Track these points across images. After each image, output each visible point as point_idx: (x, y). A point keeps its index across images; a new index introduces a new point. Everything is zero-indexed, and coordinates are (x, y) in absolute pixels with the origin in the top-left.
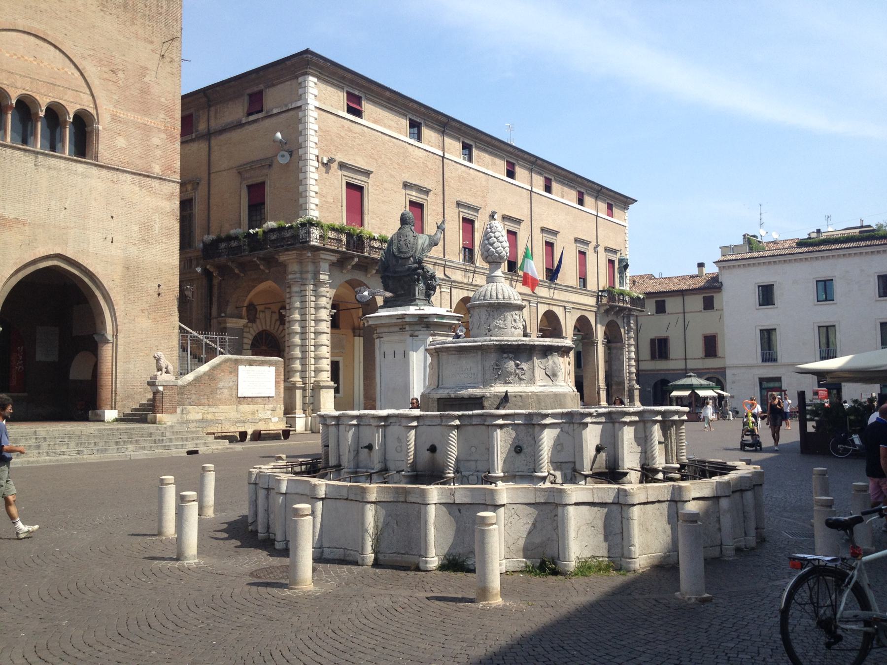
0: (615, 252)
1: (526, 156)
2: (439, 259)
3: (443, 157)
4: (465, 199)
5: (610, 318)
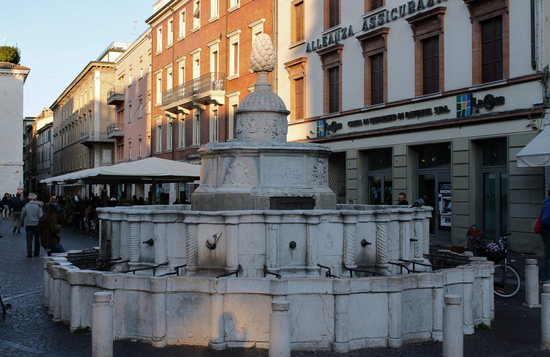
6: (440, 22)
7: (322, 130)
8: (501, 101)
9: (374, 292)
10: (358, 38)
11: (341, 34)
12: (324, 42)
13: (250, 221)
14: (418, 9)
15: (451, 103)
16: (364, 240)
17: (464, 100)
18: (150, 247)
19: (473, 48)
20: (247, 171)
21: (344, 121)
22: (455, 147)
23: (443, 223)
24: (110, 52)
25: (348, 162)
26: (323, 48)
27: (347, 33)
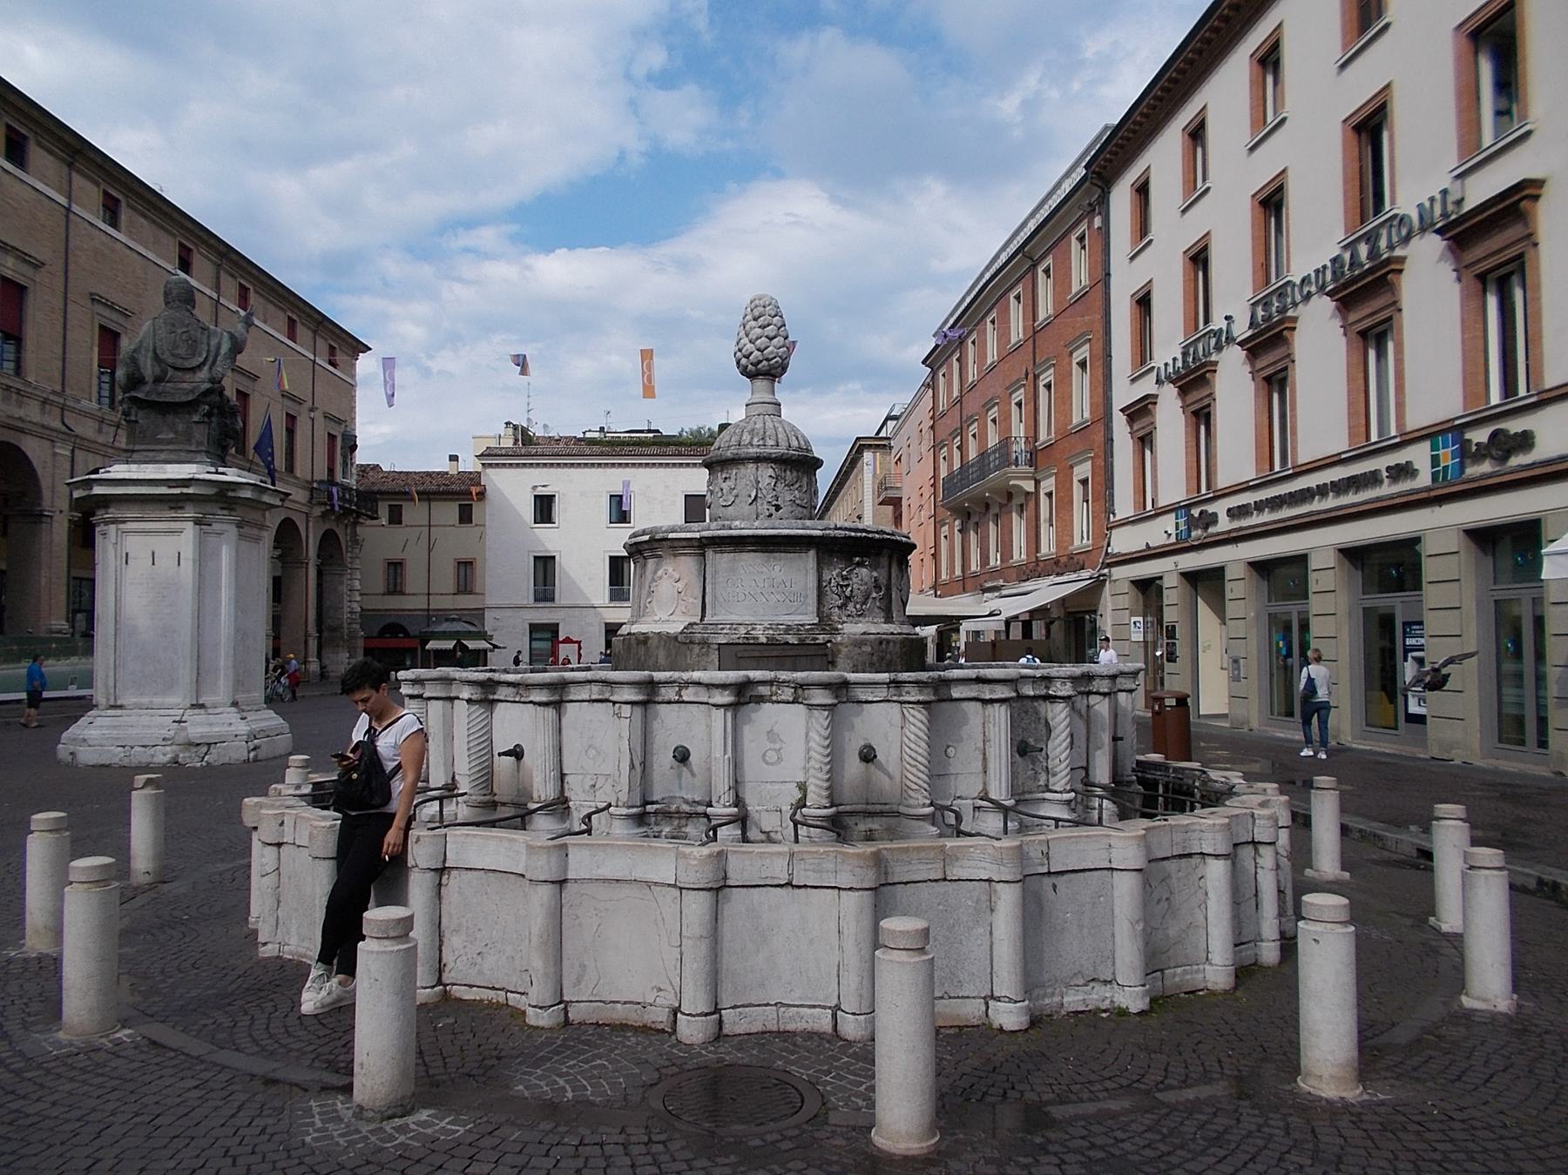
0: (339, 422)
1: (212, 241)
2: (54, 392)
3: (68, 210)
4: (101, 290)
5: (327, 526)
7: (1183, 527)
8: (1525, 441)
9: (799, 887)
11: (1213, 341)
12: (1184, 362)
13: (586, 697)
15: (1419, 455)
16: (870, 748)
19: (1463, 333)
20: (680, 585)
21: (1220, 508)
22: (1429, 547)
23: (1414, 708)
25: (1228, 586)
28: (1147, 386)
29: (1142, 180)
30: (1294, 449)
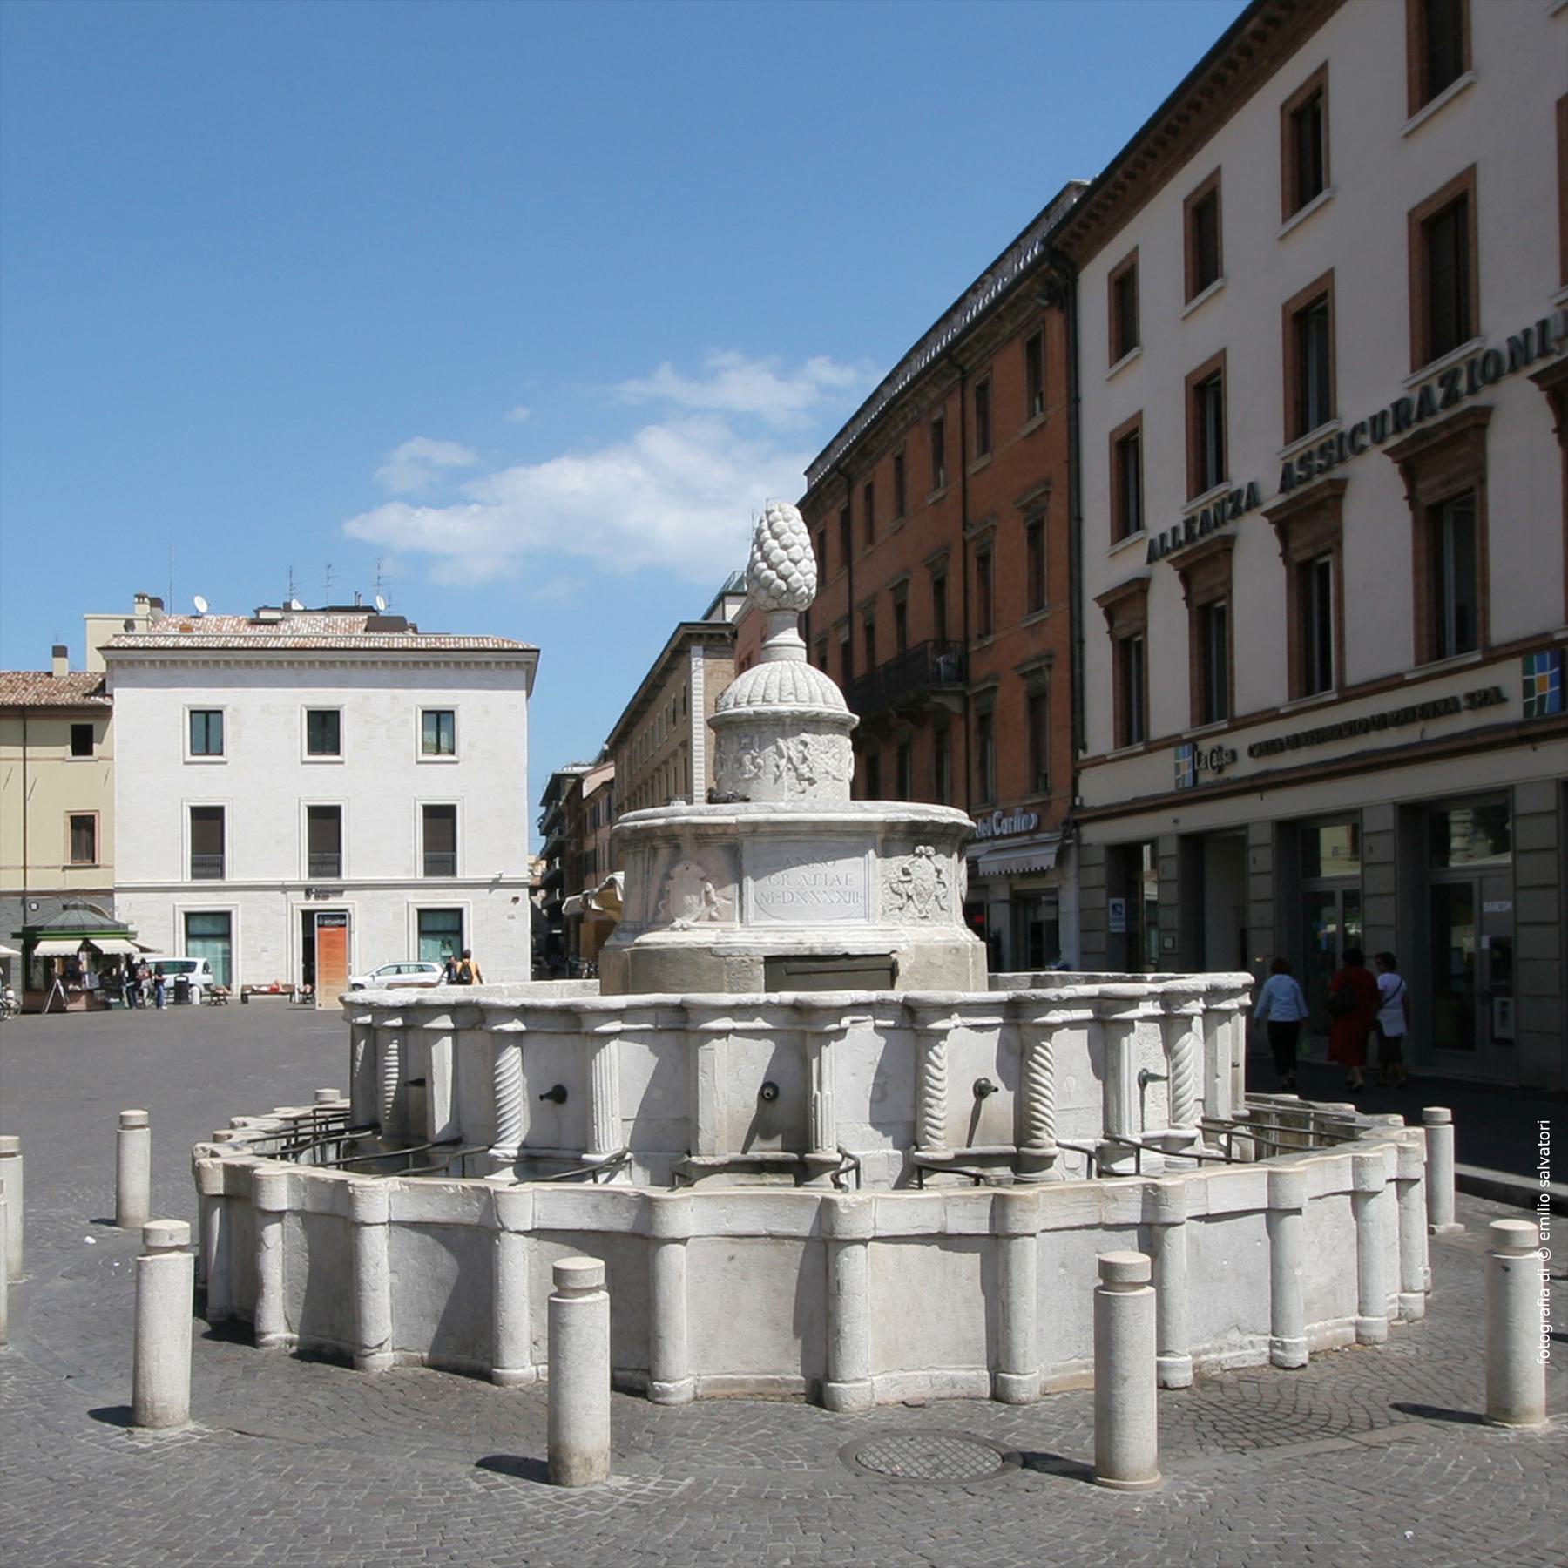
6: (1480, 447)
10: (1267, 514)
14: (1420, 418)
15: (1508, 676)
17: (1542, 669)
18: (559, 1107)
24: (727, 599)
26: (1187, 548)
27: (1243, 503)
28: (1132, 562)
29: (1127, 266)
30: (1348, 666)
